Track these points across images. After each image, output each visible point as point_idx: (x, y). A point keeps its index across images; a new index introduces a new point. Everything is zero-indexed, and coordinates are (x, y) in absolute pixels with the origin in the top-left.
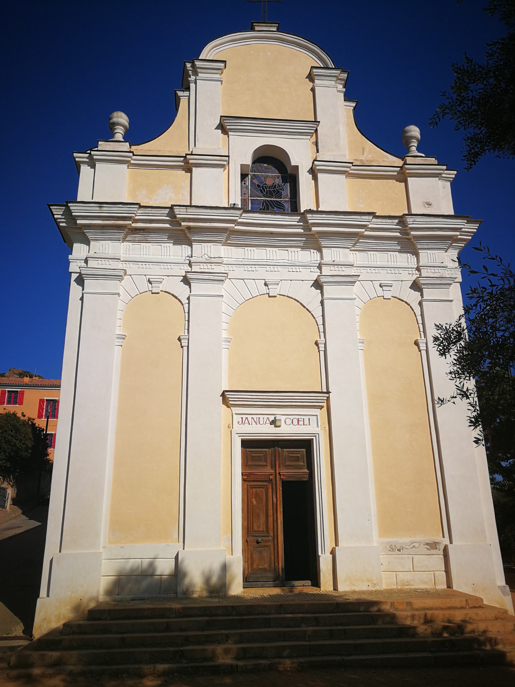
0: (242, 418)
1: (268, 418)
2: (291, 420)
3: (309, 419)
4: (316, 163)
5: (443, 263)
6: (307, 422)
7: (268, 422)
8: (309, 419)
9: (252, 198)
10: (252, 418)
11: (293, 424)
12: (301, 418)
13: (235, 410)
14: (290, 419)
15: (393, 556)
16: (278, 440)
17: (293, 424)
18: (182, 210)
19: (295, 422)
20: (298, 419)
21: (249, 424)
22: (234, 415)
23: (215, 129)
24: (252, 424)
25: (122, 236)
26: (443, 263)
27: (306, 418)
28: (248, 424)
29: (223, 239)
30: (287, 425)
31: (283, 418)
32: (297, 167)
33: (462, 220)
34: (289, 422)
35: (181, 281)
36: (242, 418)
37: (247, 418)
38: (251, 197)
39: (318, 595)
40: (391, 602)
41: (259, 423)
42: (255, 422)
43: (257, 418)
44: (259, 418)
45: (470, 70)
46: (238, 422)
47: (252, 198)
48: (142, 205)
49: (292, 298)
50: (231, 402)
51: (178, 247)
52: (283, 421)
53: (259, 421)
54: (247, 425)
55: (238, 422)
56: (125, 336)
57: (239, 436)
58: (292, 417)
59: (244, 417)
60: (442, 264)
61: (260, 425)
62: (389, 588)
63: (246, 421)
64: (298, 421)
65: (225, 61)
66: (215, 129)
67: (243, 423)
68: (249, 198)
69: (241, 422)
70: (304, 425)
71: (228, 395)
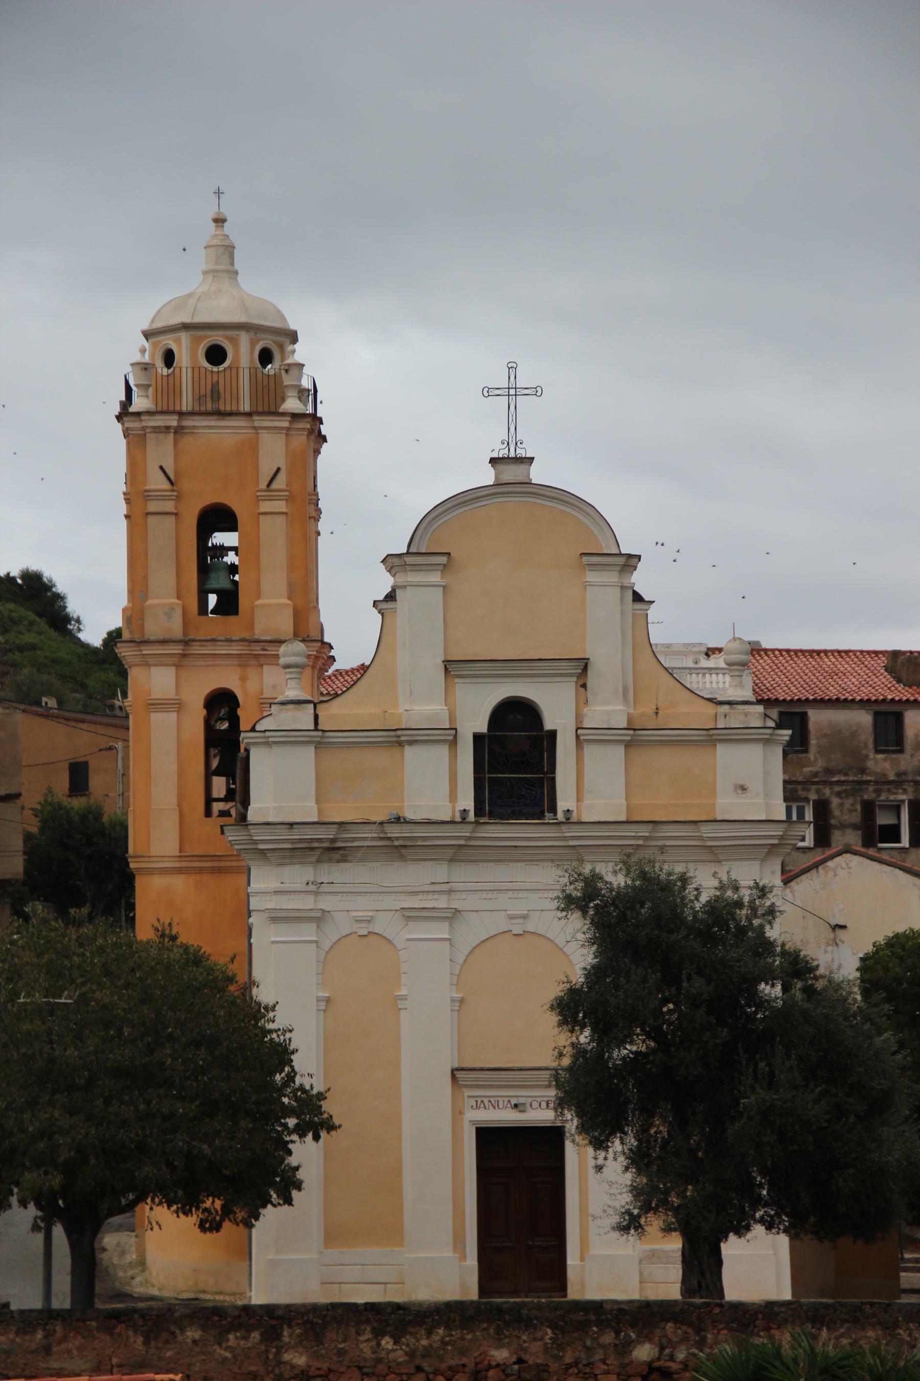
0: (477, 1101)
1: (509, 1101)
4: (580, 731)
7: (509, 1105)
9: (491, 776)
10: (490, 1101)
13: (467, 1093)
19: (544, 1105)
22: (466, 1098)
25: (314, 859)
31: (529, 1100)
32: (553, 734)
34: (535, 1105)
35: (293, 1206)
36: (477, 1101)
37: (482, 1101)
38: (489, 773)
39: (564, 1302)
40: (886, 1312)
45: (257, 1320)
46: (472, 1107)
47: (491, 776)
50: (460, 1083)
51: (294, 1198)
52: (528, 1105)
54: (482, 1110)
57: (473, 1124)
62: (643, 1298)
63: (482, 1105)
65: (449, 554)
67: (478, 1107)
68: (487, 776)
69: (475, 1107)
71: (459, 1074)
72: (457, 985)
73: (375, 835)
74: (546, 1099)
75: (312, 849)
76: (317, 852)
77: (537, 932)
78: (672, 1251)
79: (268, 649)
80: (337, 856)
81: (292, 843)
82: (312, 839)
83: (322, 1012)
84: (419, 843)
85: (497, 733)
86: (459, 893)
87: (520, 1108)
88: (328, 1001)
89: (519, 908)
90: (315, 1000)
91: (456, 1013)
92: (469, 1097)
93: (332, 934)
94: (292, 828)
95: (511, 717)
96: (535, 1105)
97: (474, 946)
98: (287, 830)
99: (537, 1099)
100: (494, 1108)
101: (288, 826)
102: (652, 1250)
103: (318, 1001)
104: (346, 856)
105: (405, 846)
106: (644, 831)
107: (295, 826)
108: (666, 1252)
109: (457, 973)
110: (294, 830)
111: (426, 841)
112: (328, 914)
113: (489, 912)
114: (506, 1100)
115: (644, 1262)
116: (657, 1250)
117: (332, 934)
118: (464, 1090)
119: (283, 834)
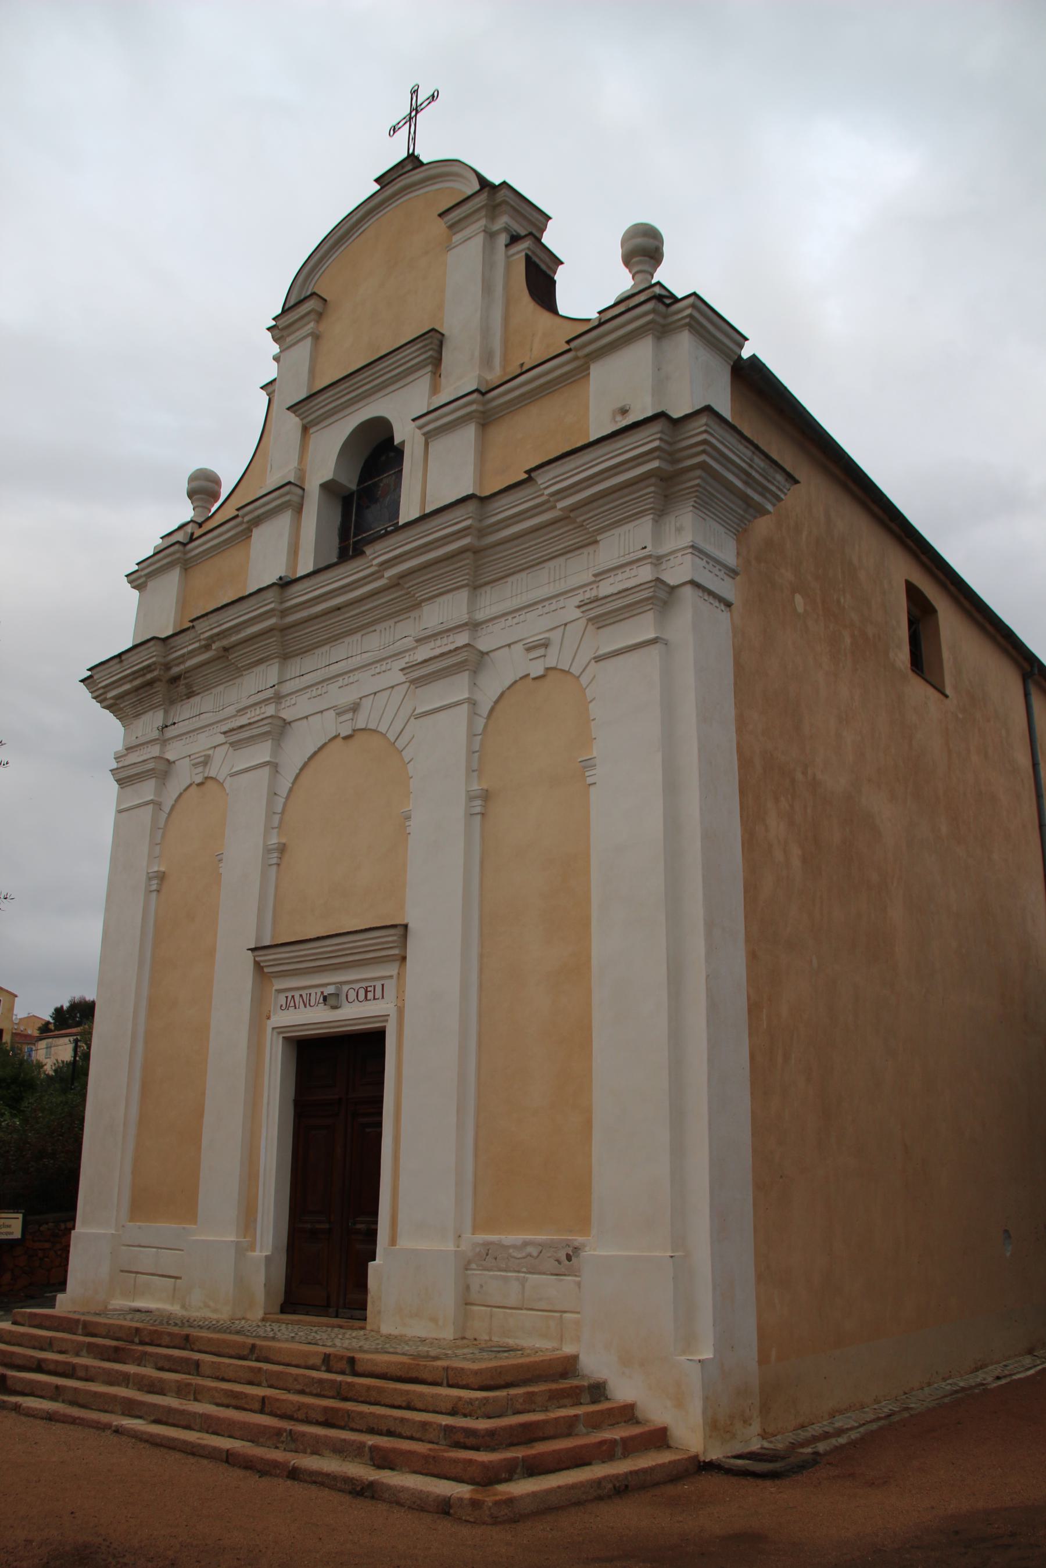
2: (356, 991)
3: (383, 985)
5: (645, 548)
6: (378, 994)
8: (383, 985)
11: (347, 1000)
12: (371, 986)
13: (279, 984)
14: (355, 990)
15: (544, 1277)
16: (348, 1033)
17: (347, 1000)
18: (142, 654)
20: (367, 987)
21: (296, 1008)
23: (80, 681)
24: (299, 1008)
26: (645, 548)
27: (297, 995)
28: (294, 1008)
29: (275, 649)
30: (349, 1002)
33: (600, 491)
34: (352, 995)
36: (287, 997)
41: (309, 1004)
42: (304, 1002)
43: (307, 994)
44: (310, 994)
46: (281, 1006)
48: (676, 415)
49: (325, 745)
50: (266, 970)
53: (310, 1000)
55: (281, 1006)
56: (655, 428)
57: (279, 1033)
58: (356, 986)
59: (290, 995)
60: (644, 550)
61: (310, 1008)
64: (366, 992)
65: (313, 294)
66: (80, 681)
69: (284, 1006)
70: (374, 999)
72: (279, 827)
73: (197, 645)
74: (364, 985)
75: (150, 683)
76: (159, 687)
77: (559, 667)
78: (514, 1247)
79: (173, 645)
80: (182, 689)
81: (131, 681)
82: (142, 669)
83: (155, 893)
84: (234, 638)
85: (366, 484)
86: (288, 698)
87: (332, 1001)
88: (162, 877)
89: (345, 697)
90: (144, 877)
91: (275, 868)
92: (279, 991)
93: (492, 686)
94: (121, 661)
95: (383, 458)
96: (352, 995)
97: (494, 700)
98: (118, 666)
99: (353, 986)
100: (305, 1006)
101: (117, 660)
102: (487, 1244)
103: (150, 879)
104: (188, 686)
105: (226, 649)
106: (463, 518)
107: (124, 657)
108: (506, 1247)
109: (280, 811)
110: (125, 663)
111: (238, 632)
112: (288, 725)
113: (319, 715)
114: (319, 991)
115: (474, 1266)
116: (492, 1243)
117: (492, 686)
118: (274, 981)
119: (115, 667)
